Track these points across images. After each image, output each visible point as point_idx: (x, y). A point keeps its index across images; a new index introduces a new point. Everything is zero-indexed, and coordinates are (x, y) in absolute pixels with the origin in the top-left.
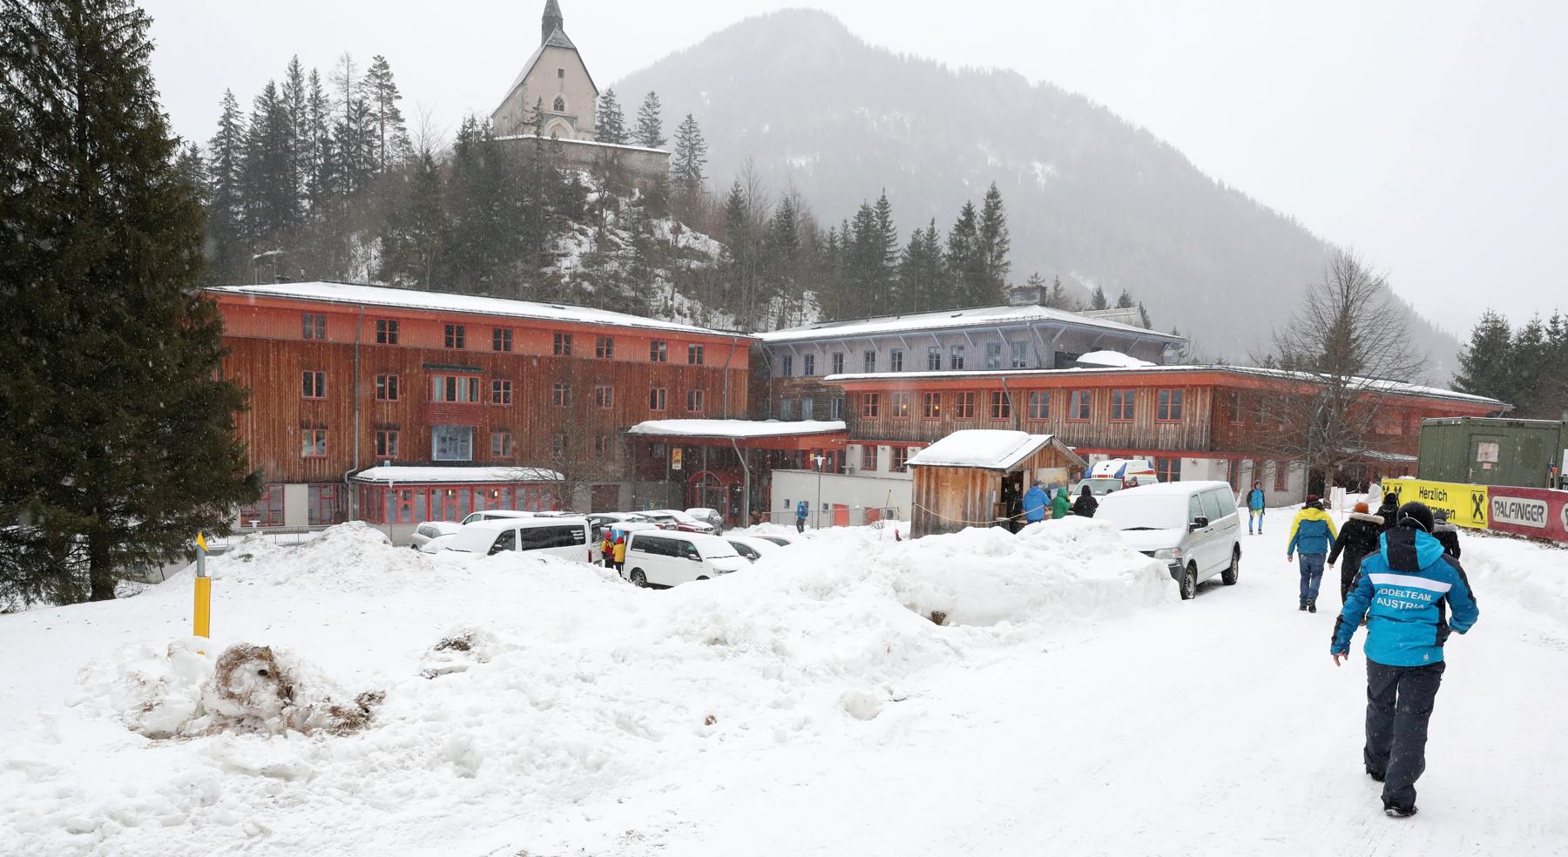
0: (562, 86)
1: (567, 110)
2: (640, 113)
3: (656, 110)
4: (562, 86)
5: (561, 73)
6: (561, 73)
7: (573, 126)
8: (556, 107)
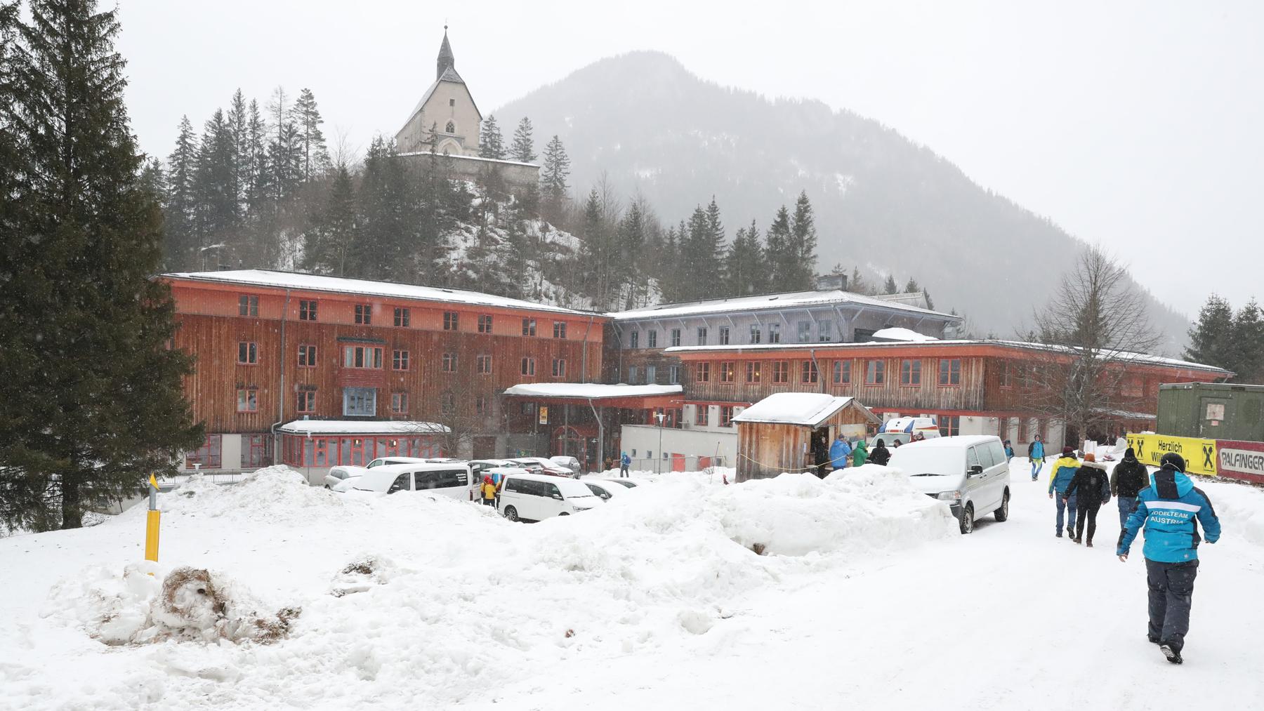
0: (453, 113)
1: (456, 133)
2: (516, 135)
3: (529, 132)
4: (453, 113)
5: (452, 102)
6: (452, 102)
7: (461, 144)
8: (448, 130)
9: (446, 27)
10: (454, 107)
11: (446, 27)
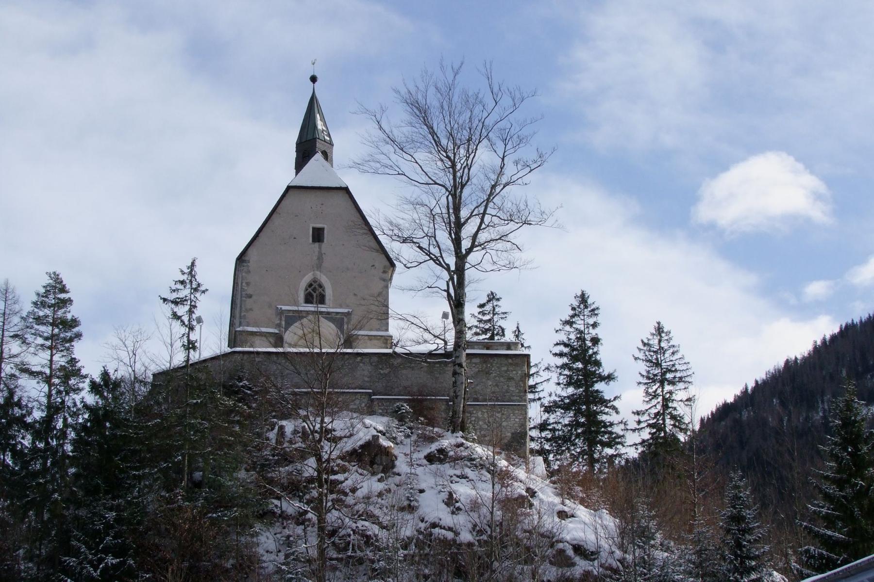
9: (314, 79)
10: (324, 245)
11: (314, 79)
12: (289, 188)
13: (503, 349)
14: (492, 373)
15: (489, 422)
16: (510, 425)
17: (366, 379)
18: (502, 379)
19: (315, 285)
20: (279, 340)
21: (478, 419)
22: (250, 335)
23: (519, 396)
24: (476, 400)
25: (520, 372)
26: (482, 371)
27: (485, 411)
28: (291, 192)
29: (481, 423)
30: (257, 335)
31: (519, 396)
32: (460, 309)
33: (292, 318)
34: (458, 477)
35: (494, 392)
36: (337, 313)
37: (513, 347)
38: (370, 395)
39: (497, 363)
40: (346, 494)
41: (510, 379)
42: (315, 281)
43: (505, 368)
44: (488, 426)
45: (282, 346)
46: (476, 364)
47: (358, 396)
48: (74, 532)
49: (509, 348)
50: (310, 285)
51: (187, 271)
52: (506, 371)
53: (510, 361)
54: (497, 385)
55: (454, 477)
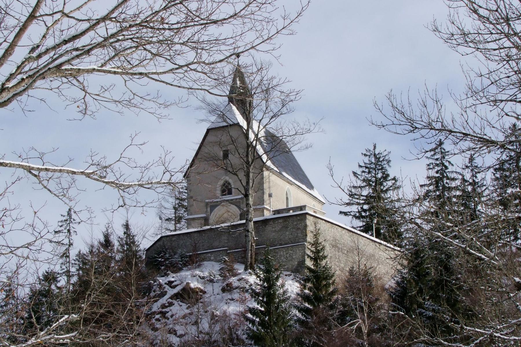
12: (208, 131)
13: (298, 211)
14: (289, 227)
15: (286, 257)
16: (297, 255)
17: (226, 241)
18: (294, 230)
19: (226, 184)
20: (206, 220)
21: (281, 256)
22: (192, 220)
23: (303, 239)
24: (281, 245)
25: (303, 224)
26: (284, 227)
27: (284, 250)
28: (210, 133)
29: (282, 258)
30: (196, 220)
31: (303, 239)
32: (247, 198)
33: (213, 206)
34: (230, 300)
35: (290, 239)
36: (236, 199)
37: (303, 209)
38: (227, 250)
39: (291, 221)
40: (168, 319)
41: (299, 229)
42: (226, 182)
43: (296, 223)
44: (286, 259)
45: (208, 225)
46: (280, 223)
47: (221, 252)
48: (429, 284)
49: (301, 210)
50: (224, 185)
51: (66, 214)
52: (296, 225)
53: (298, 218)
54: (291, 234)
55: (228, 300)
